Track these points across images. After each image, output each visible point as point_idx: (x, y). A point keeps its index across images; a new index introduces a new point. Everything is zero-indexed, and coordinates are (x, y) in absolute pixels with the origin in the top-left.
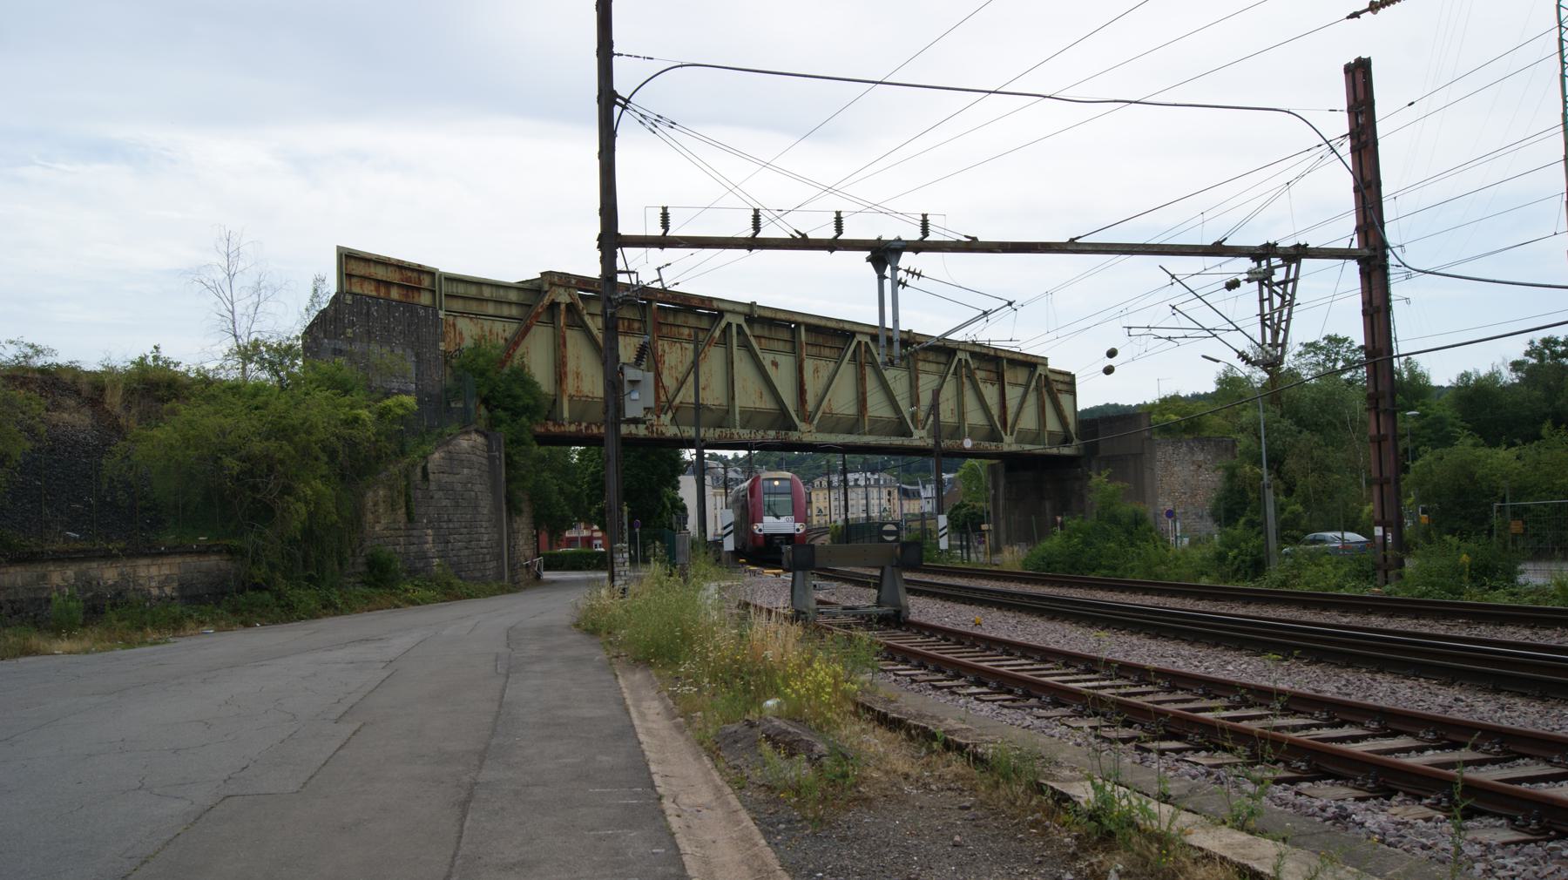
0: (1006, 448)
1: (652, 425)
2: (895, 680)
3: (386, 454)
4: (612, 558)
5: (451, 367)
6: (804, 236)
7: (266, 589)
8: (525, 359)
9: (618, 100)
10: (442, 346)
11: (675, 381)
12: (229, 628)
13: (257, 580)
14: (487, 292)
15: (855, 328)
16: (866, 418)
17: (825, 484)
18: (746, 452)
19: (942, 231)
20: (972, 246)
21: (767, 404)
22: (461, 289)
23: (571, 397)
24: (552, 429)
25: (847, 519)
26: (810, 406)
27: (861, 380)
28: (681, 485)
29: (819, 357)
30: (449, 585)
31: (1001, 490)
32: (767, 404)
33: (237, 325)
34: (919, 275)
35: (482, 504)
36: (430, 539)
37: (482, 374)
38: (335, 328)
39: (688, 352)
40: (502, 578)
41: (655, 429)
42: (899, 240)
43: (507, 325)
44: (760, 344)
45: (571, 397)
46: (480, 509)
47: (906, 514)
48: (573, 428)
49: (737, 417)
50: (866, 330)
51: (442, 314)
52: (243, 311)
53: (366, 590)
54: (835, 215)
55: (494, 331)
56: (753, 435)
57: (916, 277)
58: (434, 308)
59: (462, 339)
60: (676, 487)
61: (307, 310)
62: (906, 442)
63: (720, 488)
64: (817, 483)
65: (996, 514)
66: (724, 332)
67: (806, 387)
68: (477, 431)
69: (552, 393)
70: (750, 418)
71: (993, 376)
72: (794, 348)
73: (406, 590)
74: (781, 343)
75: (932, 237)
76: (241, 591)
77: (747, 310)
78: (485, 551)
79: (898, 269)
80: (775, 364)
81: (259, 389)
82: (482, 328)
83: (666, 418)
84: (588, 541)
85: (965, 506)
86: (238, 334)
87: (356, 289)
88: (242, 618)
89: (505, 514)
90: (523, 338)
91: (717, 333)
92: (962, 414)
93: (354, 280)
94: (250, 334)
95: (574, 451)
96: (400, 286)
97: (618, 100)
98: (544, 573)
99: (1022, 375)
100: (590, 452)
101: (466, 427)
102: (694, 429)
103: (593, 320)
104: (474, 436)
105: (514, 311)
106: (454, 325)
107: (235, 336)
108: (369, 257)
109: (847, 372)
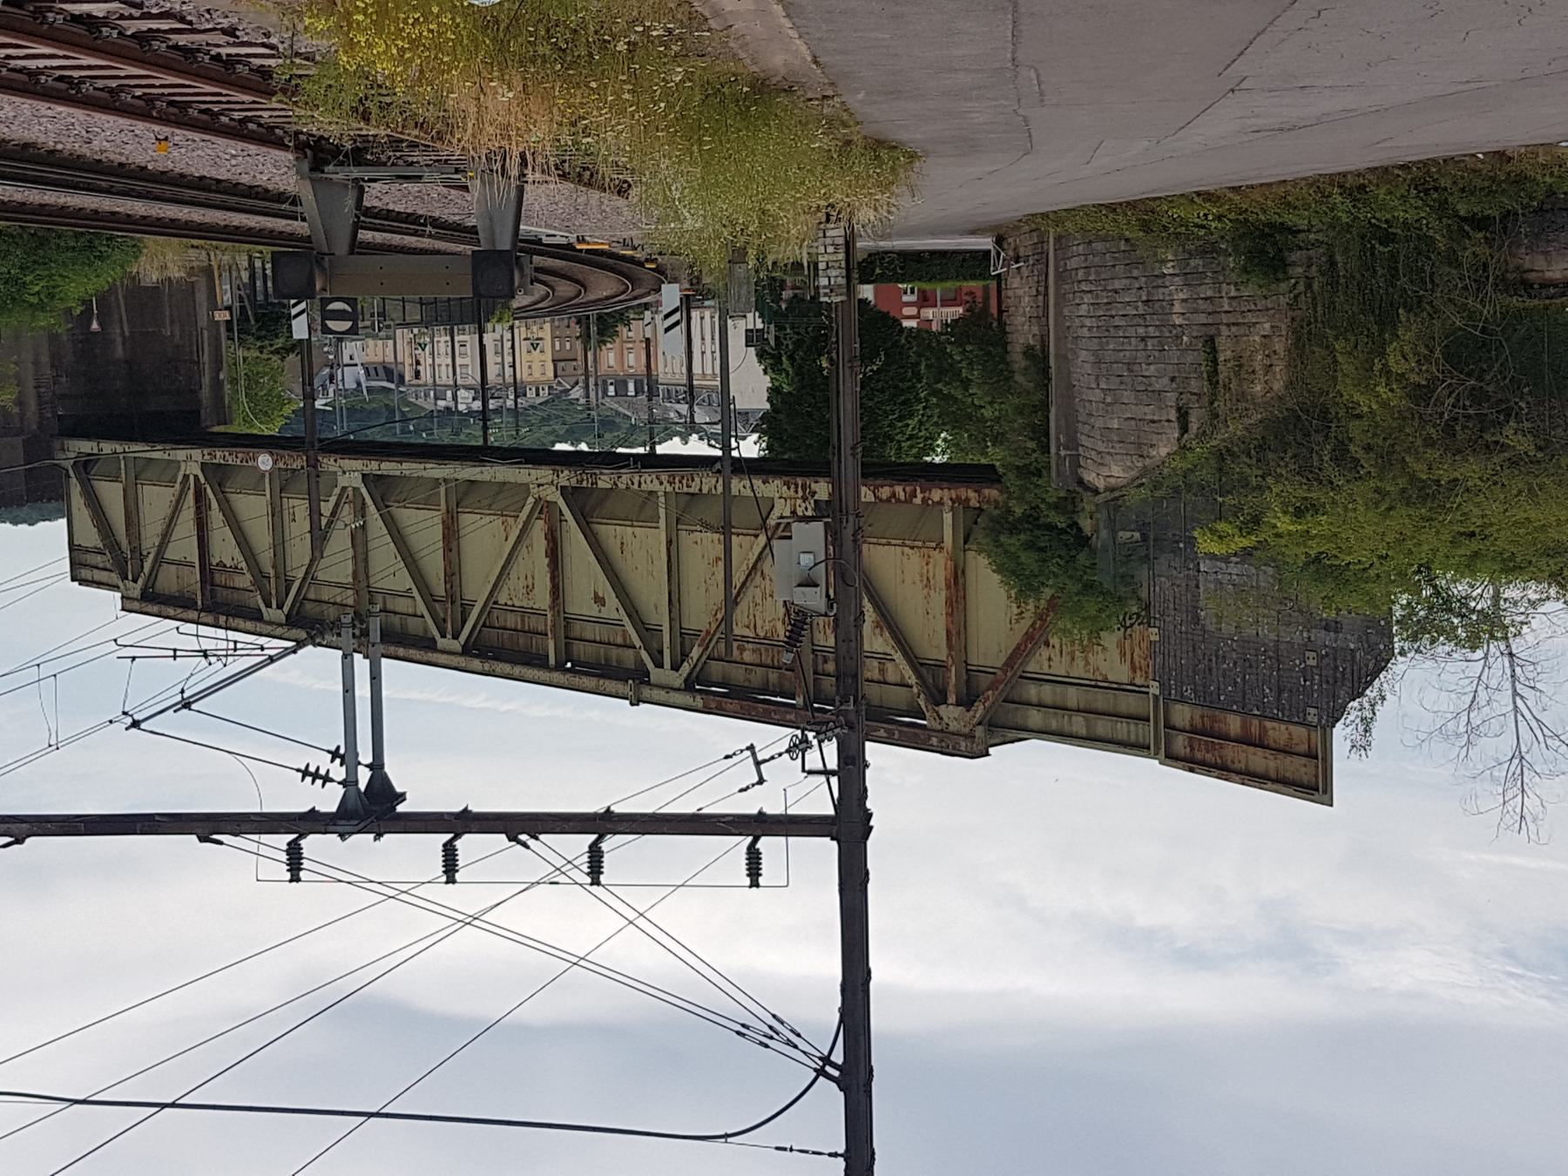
0: (197, 454)
1: (805, 499)
2: (267, 35)
3: (1249, 456)
4: (848, 278)
5: (1139, 599)
6: (513, 838)
7: (1464, 219)
8: (1016, 611)
9: (836, 1073)
10: (1154, 634)
11: (766, 571)
12: (1533, 150)
13: (1480, 235)
14: (1078, 724)
15: (462, 661)
16: (443, 506)
17: (531, 394)
18: (661, 449)
19: (263, 850)
20: (208, 827)
21: (610, 533)
22: (1122, 729)
23: (939, 546)
24: (972, 494)
25: (481, 332)
26: (539, 528)
27: (453, 572)
28: (766, 395)
29: (524, 612)
30: (1146, 227)
31: (206, 380)
32: (610, 533)
33: (1508, 671)
34: (305, 773)
35: (1088, 368)
36: (1177, 308)
37: (1089, 587)
38: (1336, 667)
39: (746, 621)
40: (1058, 239)
41: (800, 493)
42: (343, 836)
43: (1046, 670)
44: (625, 634)
45: (939, 546)
46: (1092, 359)
47: (388, 338)
48: (936, 495)
49: (662, 512)
50: (443, 658)
51: (1154, 689)
52: (1497, 696)
53: (1289, 219)
54: (458, 876)
55: (1066, 659)
56: (636, 481)
57: (312, 769)
58: (1167, 698)
59: (1121, 646)
60: (774, 392)
61: (1383, 698)
62: (373, 466)
63: (702, 387)
64: (544, 394)
65: (216, 338)
66: (685, 655)
67: (547, 561)
68: (1096, 492)
69: (970, 554)
70: (641, 510)
71: (220, 578)
72: (566, 624)
73: (1219, 218)
74: (589, 635)
75: (283, 840)
76: (1507, 215)
77: (646, 692)
78: (1084, 287)
79: (343, 783)
80: (599, 600)
81: (1469, 567)
82: (1087, 663)
83: (781, 509)
84: (925, 300)
85: (277, 352)
86: (1506, 660)
87: (1299, 732)
88: (1508, 167)
89: (1052, 350)
90: (1018, 647)
91: (695, 653)
92: (276, 513)
93: (1303, 748)
94: (1486, 657)
95: (944, 452)
96: (1227, 738)
97: (836, 1073)
98: (990, 247)
99: (168, 580)
100: (914, 451)
101: (1115, 500)
102: (734, 492)
103: (903, 677)
104: (1101, 484)
105: (1032, 692)
106: (1134, 669)
107: (1511, 655)
108: (1279, 787)
109: (476, 589)
